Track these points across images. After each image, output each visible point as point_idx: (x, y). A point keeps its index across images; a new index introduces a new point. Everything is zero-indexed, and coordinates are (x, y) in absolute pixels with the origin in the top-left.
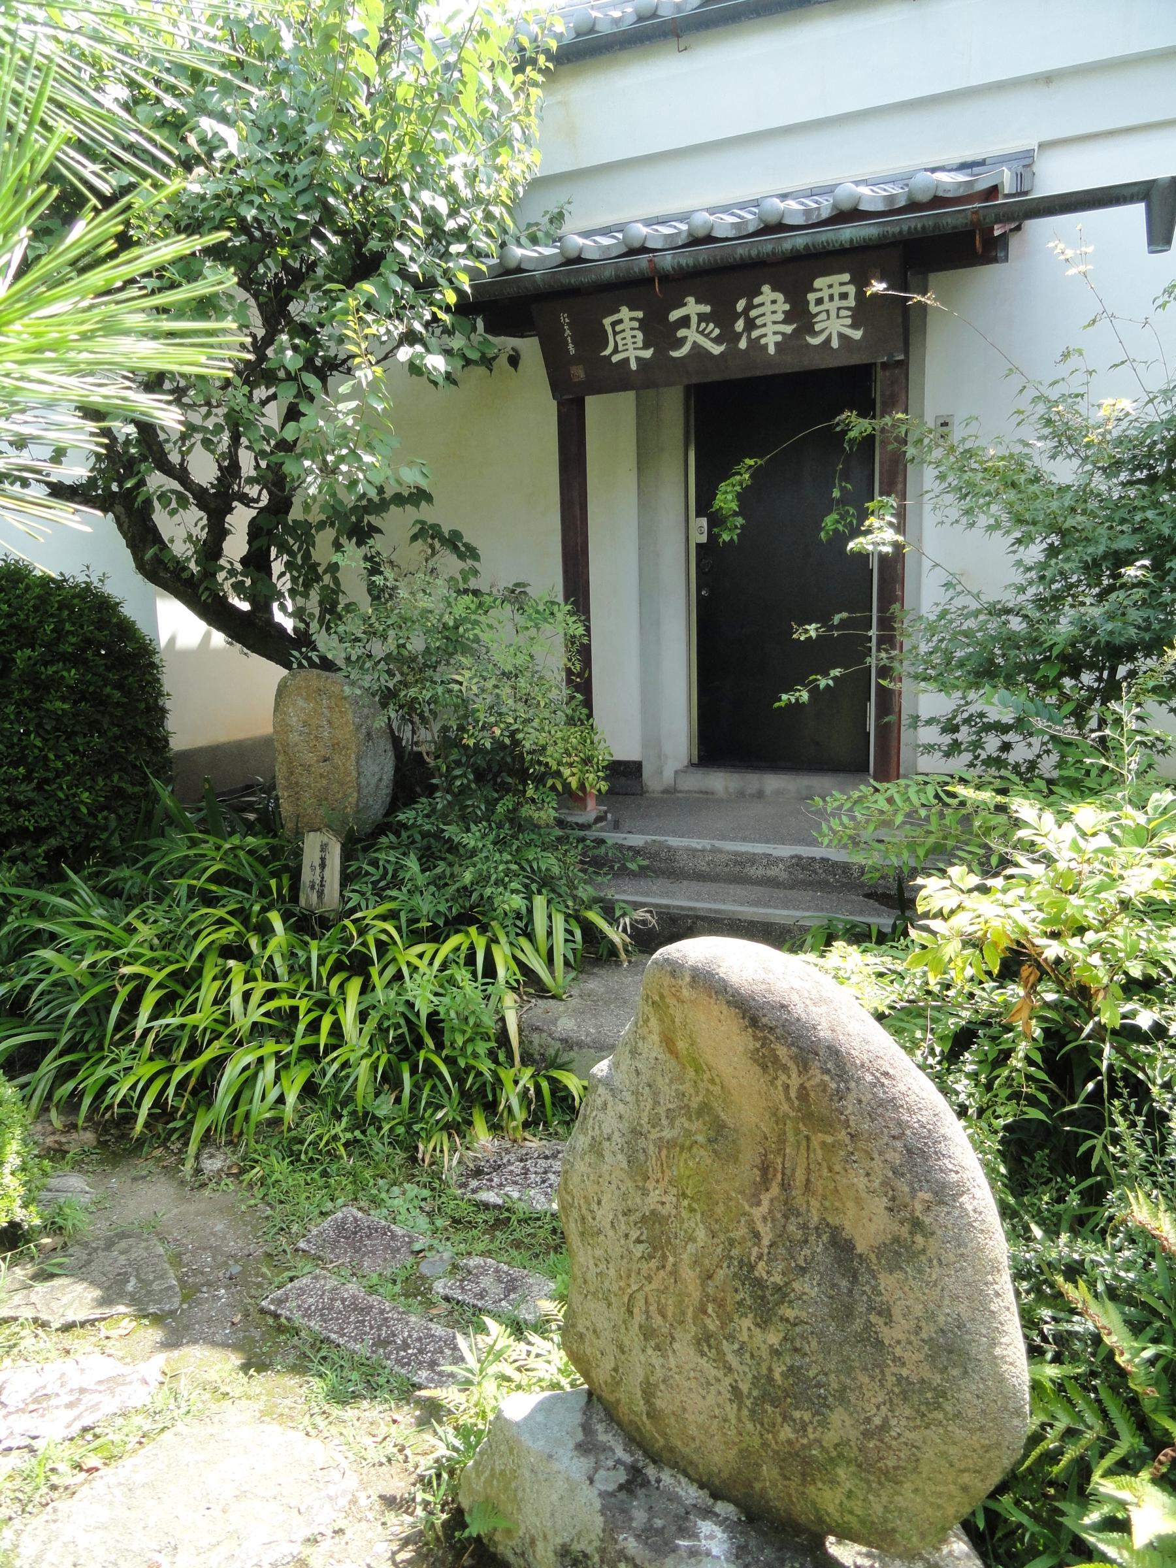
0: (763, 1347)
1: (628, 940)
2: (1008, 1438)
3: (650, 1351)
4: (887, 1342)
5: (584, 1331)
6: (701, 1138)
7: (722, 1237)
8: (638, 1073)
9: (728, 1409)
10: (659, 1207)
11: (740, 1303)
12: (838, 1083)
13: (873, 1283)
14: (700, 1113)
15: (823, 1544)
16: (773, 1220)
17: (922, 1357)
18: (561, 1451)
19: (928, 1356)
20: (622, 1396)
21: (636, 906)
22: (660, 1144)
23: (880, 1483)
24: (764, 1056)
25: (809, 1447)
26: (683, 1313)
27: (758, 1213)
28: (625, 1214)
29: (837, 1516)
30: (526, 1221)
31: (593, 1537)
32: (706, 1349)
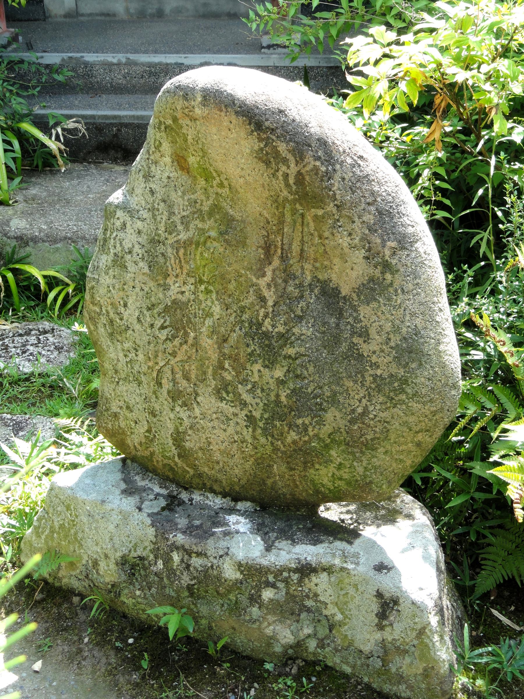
0: (271, 381)
1: (63, 147)
2: (449, 404)
3: (178, 409)
4: (365, 354)
5: (118, 410)
6: (213, 234)
7: (235, 308)
8: (152, 192)
9: (245, 432)
10: (180, 296)
11: (251, 354)
12: (327, 167)
13: (355, 315)
14: (211, 214)
15: (317, 512)
16: (276, 286)
17: (391, 359)
18: (111, 497)
19: (395, 357)
20: (156, 449)
21: (69, 117)
22: (177, 246)
23: (362, 452)
24: (267, 153)
25: (309, 442)
26: (205, 373)
27: (263, 282)
28: (149, 309)
29: (330, 485)
30: (16, 383)
31: (147, 544)
32: (225, 395)
